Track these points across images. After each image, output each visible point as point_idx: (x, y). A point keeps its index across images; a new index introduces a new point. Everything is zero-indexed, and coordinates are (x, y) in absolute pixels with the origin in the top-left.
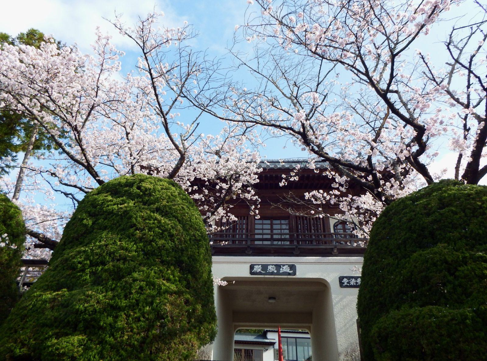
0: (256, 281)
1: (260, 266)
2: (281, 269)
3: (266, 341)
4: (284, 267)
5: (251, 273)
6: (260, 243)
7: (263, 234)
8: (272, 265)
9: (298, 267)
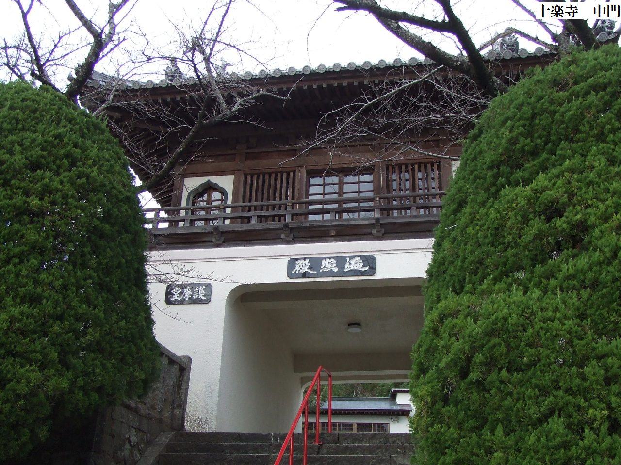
0: (308, 291)
1: (307, 261)
2: (347, 266)
3: (395, 408)
4: (353, 262)
5: (290, 275)
6: (319, 217)
7: (359, 201)
8: (330, 258)
9: (378, 258)
